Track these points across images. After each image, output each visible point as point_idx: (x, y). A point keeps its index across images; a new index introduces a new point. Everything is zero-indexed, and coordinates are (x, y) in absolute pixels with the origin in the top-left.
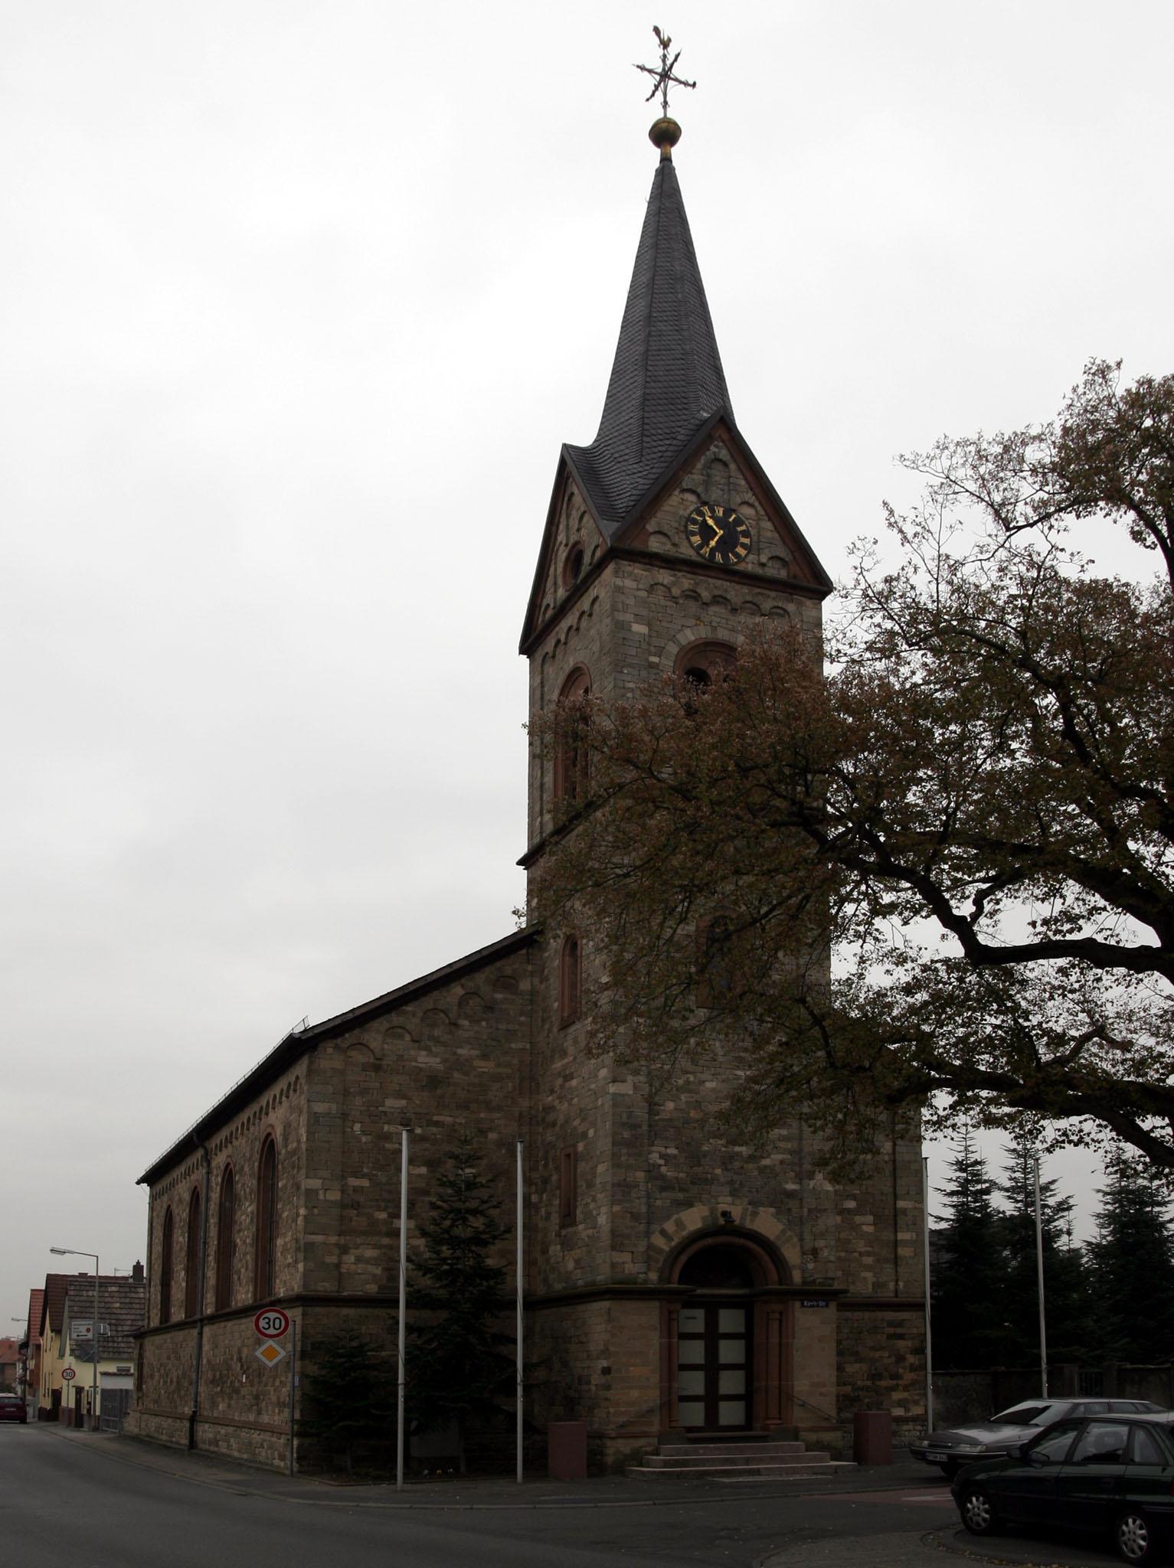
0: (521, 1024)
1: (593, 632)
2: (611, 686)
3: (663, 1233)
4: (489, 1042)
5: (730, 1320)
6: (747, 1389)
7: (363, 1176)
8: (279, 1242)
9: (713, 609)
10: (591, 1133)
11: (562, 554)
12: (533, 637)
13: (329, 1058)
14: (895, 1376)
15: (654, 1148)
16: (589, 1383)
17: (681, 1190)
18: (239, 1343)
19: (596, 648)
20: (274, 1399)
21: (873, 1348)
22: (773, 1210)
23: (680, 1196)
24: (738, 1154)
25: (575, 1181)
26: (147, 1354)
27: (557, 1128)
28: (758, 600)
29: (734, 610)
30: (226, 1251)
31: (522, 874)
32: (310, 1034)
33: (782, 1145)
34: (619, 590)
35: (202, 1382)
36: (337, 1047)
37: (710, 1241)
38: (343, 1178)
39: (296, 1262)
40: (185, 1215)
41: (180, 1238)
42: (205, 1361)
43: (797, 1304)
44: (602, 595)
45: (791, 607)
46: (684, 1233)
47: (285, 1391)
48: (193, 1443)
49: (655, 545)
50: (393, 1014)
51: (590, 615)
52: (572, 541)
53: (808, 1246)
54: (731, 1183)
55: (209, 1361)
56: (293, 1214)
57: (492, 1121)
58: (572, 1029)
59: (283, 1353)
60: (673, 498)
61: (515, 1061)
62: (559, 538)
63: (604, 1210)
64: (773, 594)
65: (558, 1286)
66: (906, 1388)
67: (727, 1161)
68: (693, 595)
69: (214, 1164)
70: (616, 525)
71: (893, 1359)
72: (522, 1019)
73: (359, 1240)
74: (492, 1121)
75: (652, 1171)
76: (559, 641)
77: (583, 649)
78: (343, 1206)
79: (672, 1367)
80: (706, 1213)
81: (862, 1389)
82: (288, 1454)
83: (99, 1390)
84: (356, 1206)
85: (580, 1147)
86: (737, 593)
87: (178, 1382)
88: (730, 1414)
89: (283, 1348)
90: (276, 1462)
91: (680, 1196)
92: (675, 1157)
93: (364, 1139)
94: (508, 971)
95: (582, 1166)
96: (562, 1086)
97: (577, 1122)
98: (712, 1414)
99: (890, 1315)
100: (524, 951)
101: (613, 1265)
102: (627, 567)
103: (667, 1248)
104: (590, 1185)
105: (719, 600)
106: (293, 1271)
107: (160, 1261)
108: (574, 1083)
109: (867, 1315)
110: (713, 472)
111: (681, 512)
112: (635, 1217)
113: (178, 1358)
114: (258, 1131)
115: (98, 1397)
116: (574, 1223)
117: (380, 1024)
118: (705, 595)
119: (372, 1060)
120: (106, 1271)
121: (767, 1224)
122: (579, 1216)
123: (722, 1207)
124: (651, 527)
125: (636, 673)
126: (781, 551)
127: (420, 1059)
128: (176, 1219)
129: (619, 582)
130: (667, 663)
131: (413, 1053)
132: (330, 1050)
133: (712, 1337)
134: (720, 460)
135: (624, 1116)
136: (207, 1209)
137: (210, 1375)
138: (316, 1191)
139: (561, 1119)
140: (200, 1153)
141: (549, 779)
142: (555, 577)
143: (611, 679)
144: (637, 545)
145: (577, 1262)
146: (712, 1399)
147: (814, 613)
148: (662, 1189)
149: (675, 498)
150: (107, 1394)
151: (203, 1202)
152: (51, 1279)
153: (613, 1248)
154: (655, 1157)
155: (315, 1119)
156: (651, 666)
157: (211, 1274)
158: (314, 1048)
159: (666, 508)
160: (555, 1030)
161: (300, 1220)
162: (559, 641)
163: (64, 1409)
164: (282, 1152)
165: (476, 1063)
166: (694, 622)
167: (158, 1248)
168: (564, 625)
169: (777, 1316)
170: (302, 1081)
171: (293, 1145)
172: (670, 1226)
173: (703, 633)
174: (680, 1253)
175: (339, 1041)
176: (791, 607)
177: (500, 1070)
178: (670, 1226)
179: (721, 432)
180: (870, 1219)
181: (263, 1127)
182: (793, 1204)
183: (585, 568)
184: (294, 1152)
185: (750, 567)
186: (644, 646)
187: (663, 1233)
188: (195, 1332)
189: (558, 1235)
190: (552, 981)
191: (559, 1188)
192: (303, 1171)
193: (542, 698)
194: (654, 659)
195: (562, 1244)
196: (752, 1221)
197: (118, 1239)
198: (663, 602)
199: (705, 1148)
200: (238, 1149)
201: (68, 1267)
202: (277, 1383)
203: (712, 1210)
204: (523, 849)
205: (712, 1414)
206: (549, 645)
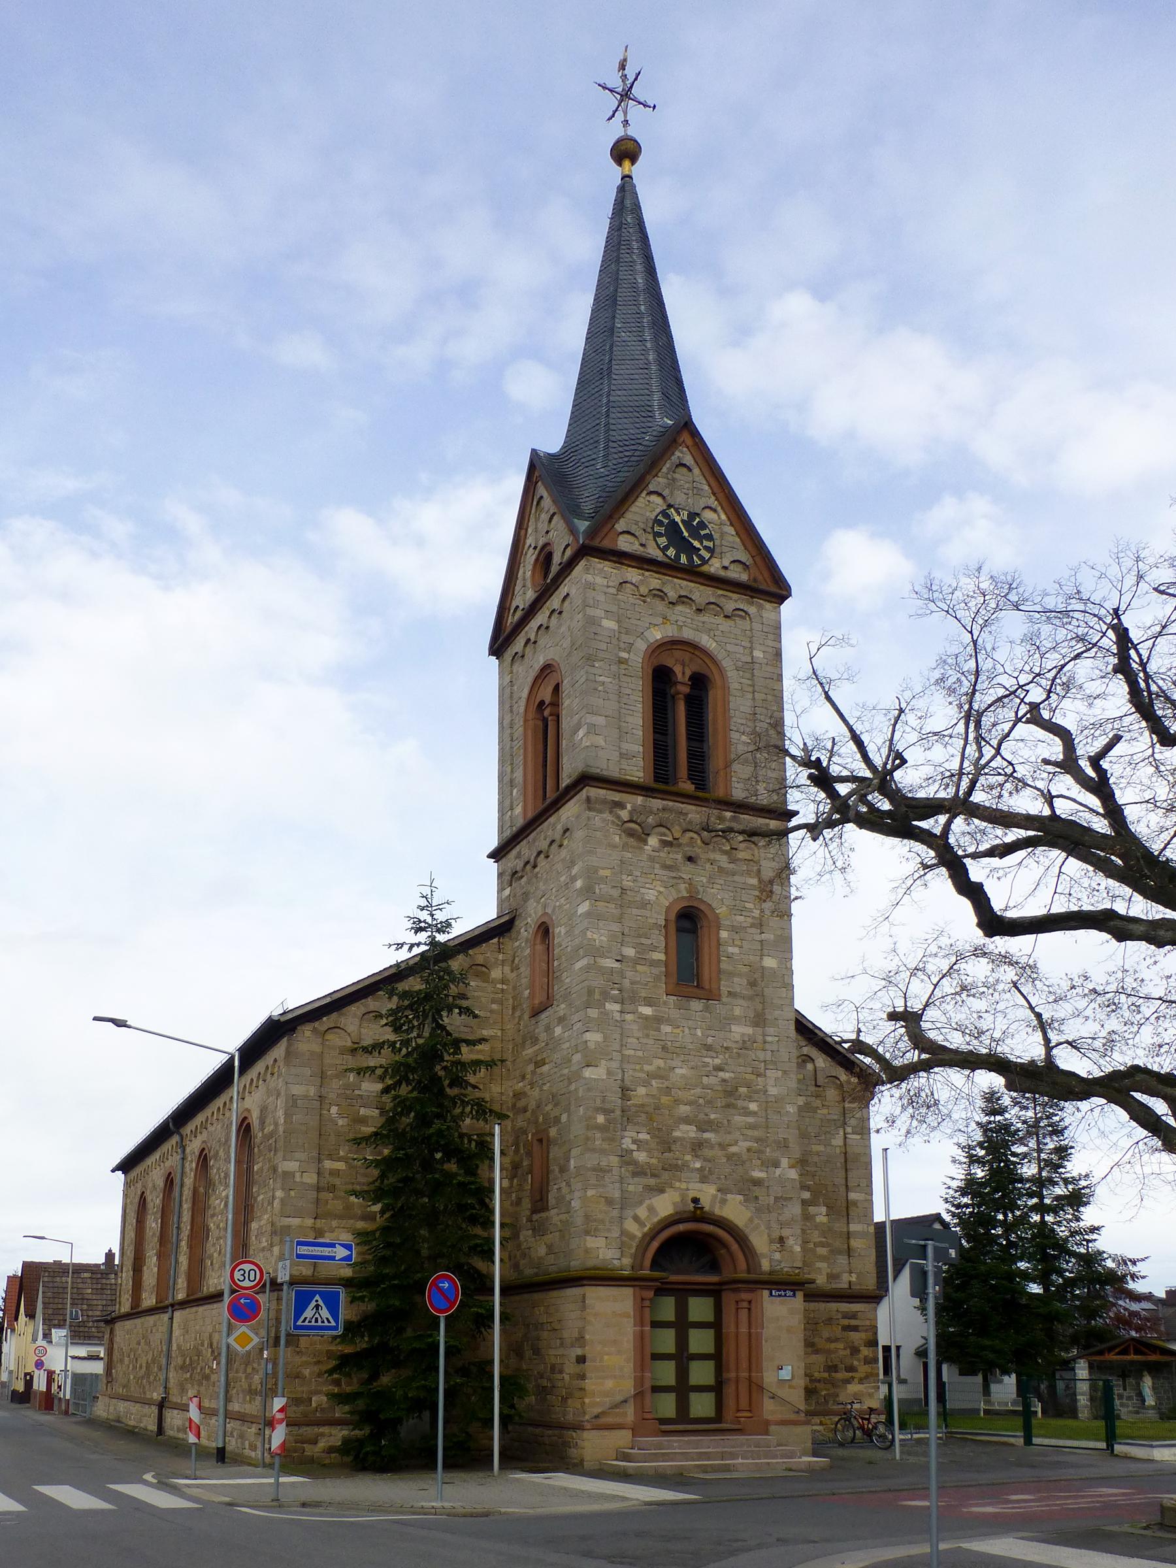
0: (491, 1011)
1: (563, 629)
3: (636, 1218)
5: (700, 1309)
6: (717, 1380)
7: (339, 1159)
8: (254, 1225)
9: (679, 608)
10: (564, 1118)
11: (530, 558)
13: (306, 1040)
14: (851, 1369)
15: (626, 1134)
17: (653, 1175)
18: (210, 1329)
19: (566, 643)
20: (245, 1386)
21: (829, 1340)
22: (741, 1197)
23: (652, 1181)
24: (707, 1141)
25: (548, 1167)
26: (117, 1339)
27: (528, 1114)
28: (722, 601)
29: (699, 610)
30: (199, 1234)
31: (492, 867)
32: (290, 1016)
33: (750, 1133)
34: (591, 586)
35: (172, 1368)
36: (315, 1030)
37: (681, 1227)
38: (320, 1161)
39: (272, 1245)
40: (158, 1202)
41: (153, 1224)
42: (174, 1347)
43: (766, 1293)
44: (573, 592)
45: (752, 610)
46: (656, 1220)
47: (257, 1378)
48: (160, 1430)
49: (625, 544)
51: (560, 613)
52: (541, 543)
53: (776, 1235)
54: (701, 1169)
55: (179, 1347)
56: (271, 1200)
58: (543, 1016)
59: (256, 1340)
60: (640, 499)
62: (528, 542)
64: (735, 596)
65: (529, 1272)
66: (861, 1381)
67: (697, 1147)
68: (660, 594)
69: (188, 1150)
70: (587, 523)
71: (848, 1351)
72: (494, 1006)
73: (334, 1223)
75: (625, 1157)
76: (529, 640)
77: (552, 643)
78: (319, 1189)
79: (648, 1357)
80: (678, 1199)
81: (819, 1381)
82: (259, 1444)
84: (332, 1188)
86: (701, 593)
87: (147, 1368)
88: (702, 1405)
89: (257, 1334)
90: (247, 1452)
91: (652, 1181)
92: (647, 1142)
93: (340, 1122)
94: (480, 959)
95: (555, 1152)
96: (533, 1073)
97: (550, 1107)
98: (683, 1406)
99: (845, 1307)
100: (495, 940)
103: (639, 1235)
104: (563, 1169)
105: (683, 599)
106: (268, 1254)
107: (132, 1247)
108: (545, 1068)
109: (822, 1306)
110: (677, 476)
111: (648, 514)
112: (609, 1202)
113: (148, 1343)
115: (69, 1381)
116: (545, 1209)
117: (356, 1009)
118: (672, 595)
119: (349, 1044)
120: (81, 1258)
121: (735, 1210)
122: (552, 1201)
123: (692, 1194)
124: (621, 526)
126: (744, 557)
128: (150, 1205)
129: (590, 578)
132: (308, 1034)
133: (682, 1325)
134: (684, 465)
135: (598, 1101)
136: (181, 1195)
137: (180, 1361)
138: (293, 1174)
139: (532, 1105)
140: (175, 1139)
141: (519, 775)
142: (524, 579)
144: (606, 544)
145: (550, 1247)
146: (683, 1389)
147: (772, 616)
148: (635, 1174)
149: (641, 501)
150: (79, 1380)
151: (177, 1189)
152: (27, 1266)
154: (627, 1143)
155: (293, 1101)
156: (621, 661)
157: (183, 1260)
158: (293, 1030)
159: (633, 509)
160: (526, 1017)
161: (276, 1203)
162: (529, 640)
163: (36, 1392)
164: (258, 1134)
167: (131, 1235)
168: (534, 624)
169: (745, 1304)
170: (281, 1063)
173: (670, 632)
174: (653, 1238)
175: (317, 1024)
176: (752, 610)
178: (642, 1212)
179: (685, 437)
180: (824, 1210)
182: (757, 1191)
183: (555, 569)
184: (271, 1135)
185: (712, 570)
186: (614, 641)
187: (636, 1218)
188: (165, 1317)
189: (530, 1220)
190: (522, 969)
191: (530, 1172)
193: (511, 697)
194: (624, 655)
195: (534, 1230)
196: (721, 1208)
197: (91, 1230)
198: (632, 600)
199: (677, 1134)
200: (216, 1130)
201: (45, 1254)
202: (249, 1370)
204: (493, 843)
205: (683, 1406)
206: (518, 645)
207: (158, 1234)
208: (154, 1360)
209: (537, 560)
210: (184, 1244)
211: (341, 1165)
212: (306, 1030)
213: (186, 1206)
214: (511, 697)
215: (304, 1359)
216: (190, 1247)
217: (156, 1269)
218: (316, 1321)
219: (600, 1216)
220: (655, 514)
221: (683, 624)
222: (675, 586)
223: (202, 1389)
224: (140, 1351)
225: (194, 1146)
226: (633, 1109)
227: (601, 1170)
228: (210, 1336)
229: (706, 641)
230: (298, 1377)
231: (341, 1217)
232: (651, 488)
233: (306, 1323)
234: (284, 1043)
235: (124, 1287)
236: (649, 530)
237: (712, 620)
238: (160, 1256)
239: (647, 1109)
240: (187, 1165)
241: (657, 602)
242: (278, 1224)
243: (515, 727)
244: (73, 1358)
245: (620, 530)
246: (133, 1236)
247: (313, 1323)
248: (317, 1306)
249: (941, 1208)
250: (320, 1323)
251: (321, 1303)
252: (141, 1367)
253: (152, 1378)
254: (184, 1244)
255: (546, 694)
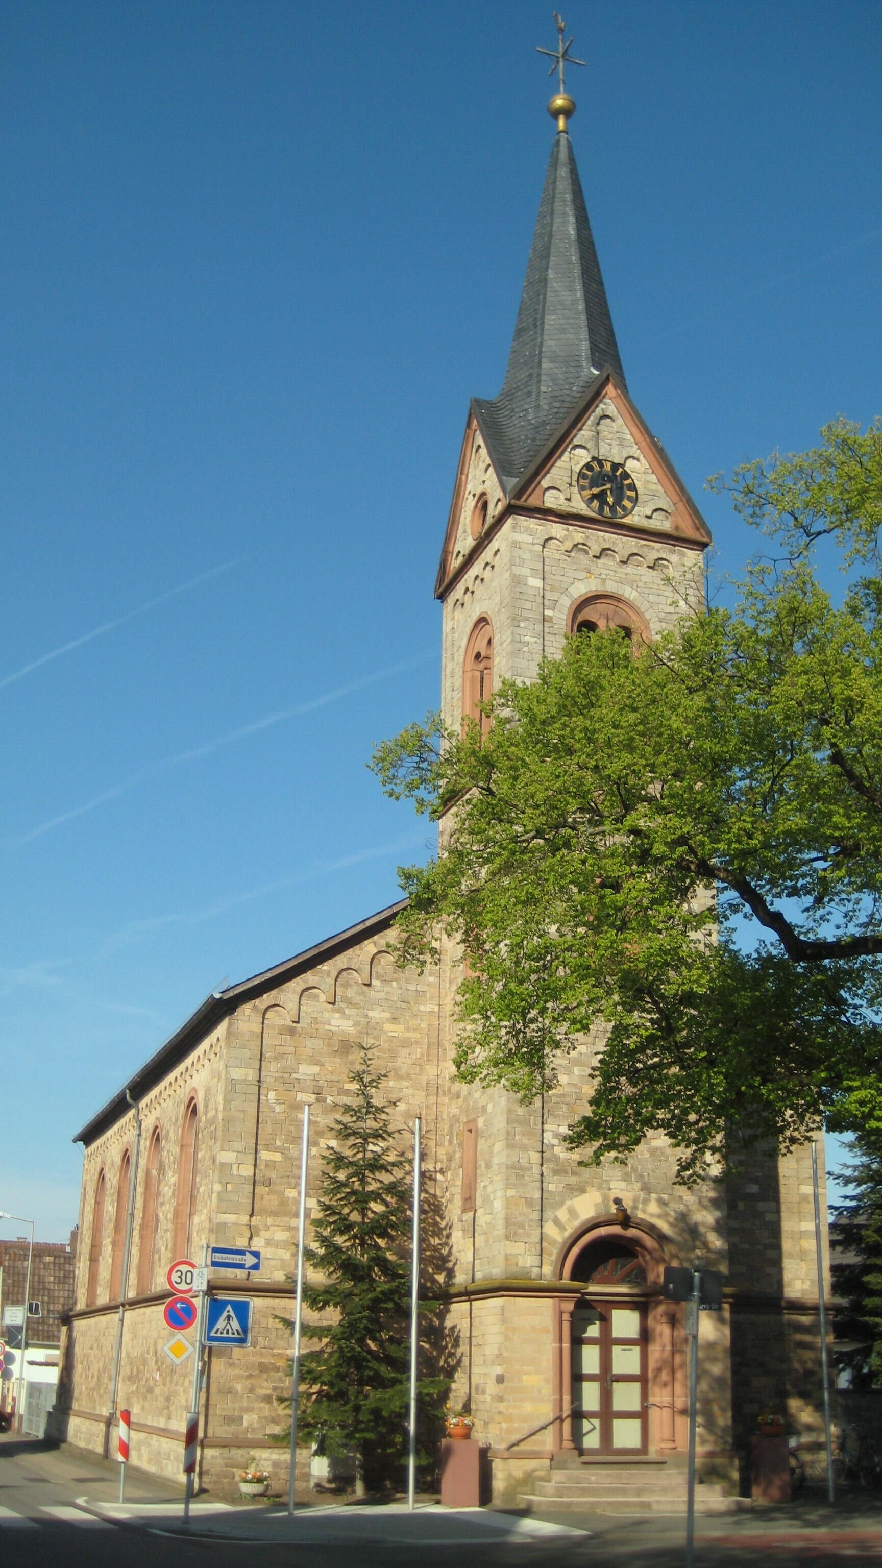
0: (429, 985)
2: (509, 640)
3: (557, 1222)
4: (399, 1004)
7: (276, 1150)
8: (196, 1219)
9: (603, 561)
10: (490, 1108)
12: (443, 586)
16: (484, 1392)
19: (497, 599)
23: (573, 1180)
27: (461, 1100)
30: (150, 1224)
34: (516, 545)
37: (603, 1231)
41: (110, 1208)
42: (124, 1355)
49: (552, 500)
50: (308, 973)
57: (401, 1090)
61: (424, 1025)
62: (469, 487)
63: (500, 1194)
73: (270, 1221)
74: (401, 1090)
83: (25, 1383)
85: (480, 1122)
86: (625, 544)
91: (573, 1180)
93: (278, 1109)
101: (507, 1257)
102: (523, 521)
104: (488, 1166)
113: (100, 1348)
114: (183, 1094)
122: (479, 1201)
123: (614, 1194)
124: (545, 483)
125: (532, 627)
127: (333, 1022)
130: (561, 616)
131: (326, 1014)
134: (608, 417)
143: (509, 632)
144: (533, 501)
153: (507, 1238)
159: (559, 463)
162: (467, 589)
165: (387, 1027)
166: (585, 574)
170: (222, 1043)
171: (211, 1114)
172: (562, 1214)
175: (257, 1001)
177: (408, 1035)
178: (562, 1214)
181: (188, 1089)
187: (557, 1222)
188: (116, 1317)
191: (461, 1166)
192: (219, 1143)
203: (605, 1199)
206: (458, 592)
207: (114, 1219)
208: (105, 1368)
209: (476, 506)
210: (136, 1233)
211: (277, 1157)
212: (246, 1010)
213: (140, 1190)
214: (453, 644)
215: (237, 1371)
216: (142, 1237)
217: (110, 1261)
218: (228, 1333)
219: (520, 1219)
220: (579, 467)
221: (605, 577)
222: (599, 538)
223: (147, 1404)
224: (92, 1358)
225: (148, 1122)
226: (554, 1099)
227: (521, 1168)
228: (155, 1344)
229: (629, 593)
230: (229, 1392)
231: (275, 1214)
232: (576, 442)
233: (219, 1335)
234: (224, 1024)
235: (81, 1279)
236: (574, 483)
237: (635, 572)
238: (114, 1244)
239: (568, 1099)
240: (142, 1142)
241: (581, 556)
242: (215, 1221)
243: (456, 678)
244: (32, 1363)
245: (546, 486)
246: (91, 1218)
247: (225, 1335)
248: (229, 1317)
249: (11, 1367)
250: (230, 1335)
251: (232, 1313)
252: (92, 1377)
253: (102, 1391)
254: (136, 1233)
255: (481, 646)
